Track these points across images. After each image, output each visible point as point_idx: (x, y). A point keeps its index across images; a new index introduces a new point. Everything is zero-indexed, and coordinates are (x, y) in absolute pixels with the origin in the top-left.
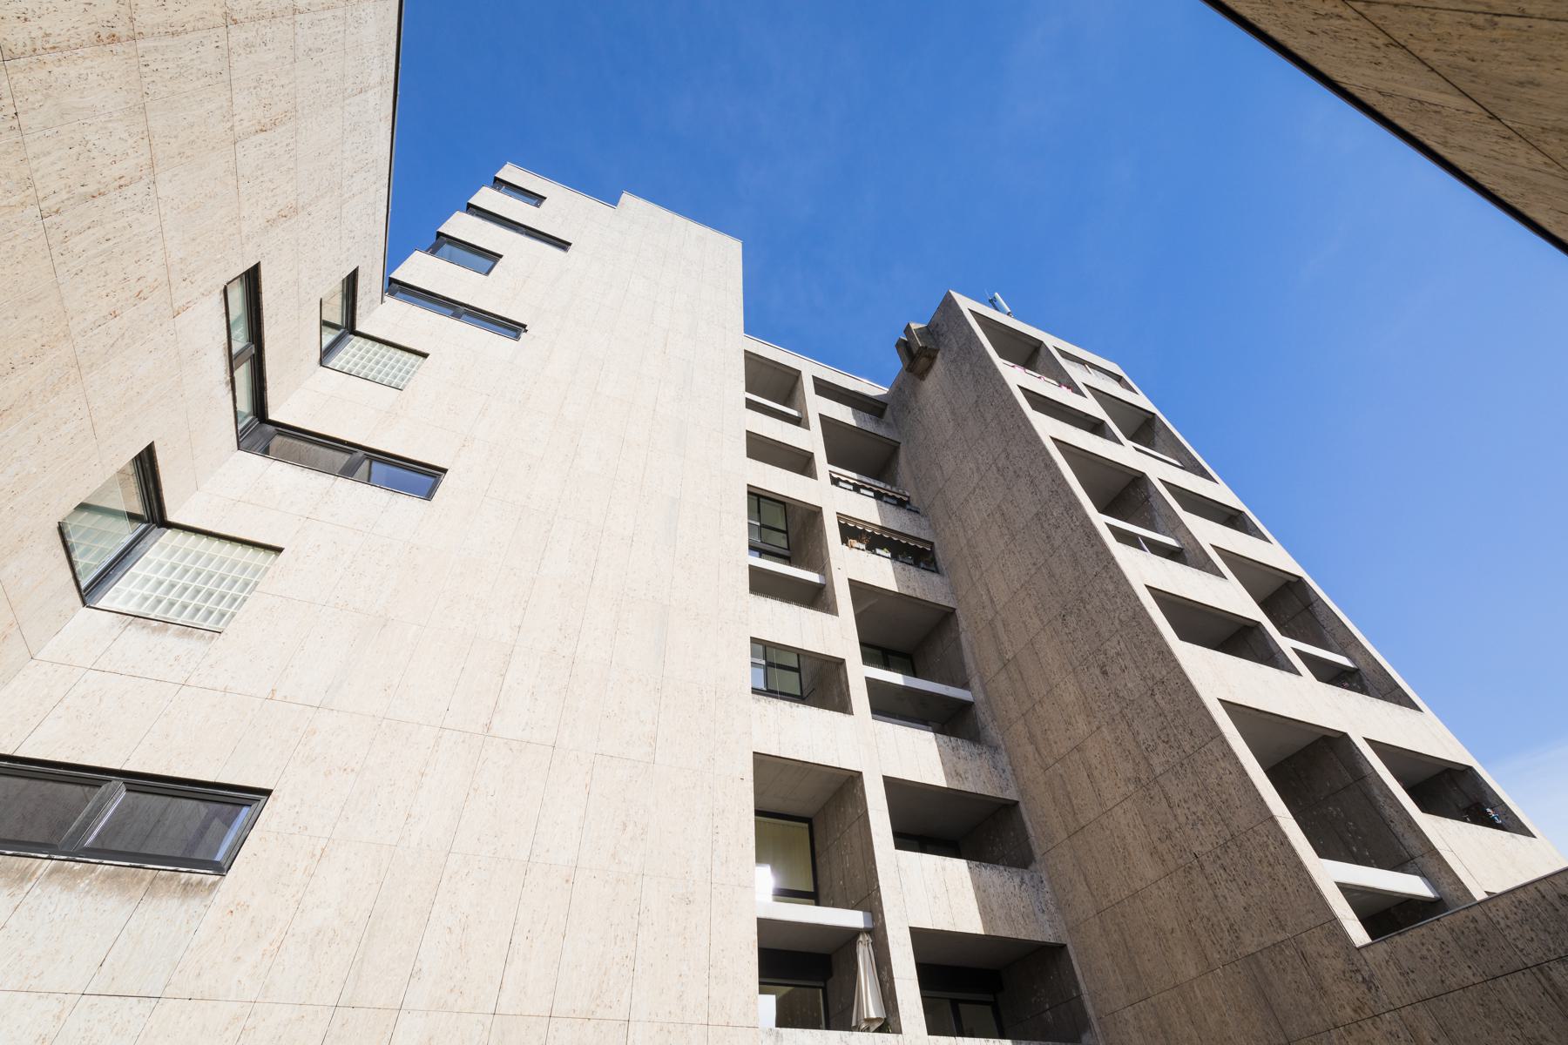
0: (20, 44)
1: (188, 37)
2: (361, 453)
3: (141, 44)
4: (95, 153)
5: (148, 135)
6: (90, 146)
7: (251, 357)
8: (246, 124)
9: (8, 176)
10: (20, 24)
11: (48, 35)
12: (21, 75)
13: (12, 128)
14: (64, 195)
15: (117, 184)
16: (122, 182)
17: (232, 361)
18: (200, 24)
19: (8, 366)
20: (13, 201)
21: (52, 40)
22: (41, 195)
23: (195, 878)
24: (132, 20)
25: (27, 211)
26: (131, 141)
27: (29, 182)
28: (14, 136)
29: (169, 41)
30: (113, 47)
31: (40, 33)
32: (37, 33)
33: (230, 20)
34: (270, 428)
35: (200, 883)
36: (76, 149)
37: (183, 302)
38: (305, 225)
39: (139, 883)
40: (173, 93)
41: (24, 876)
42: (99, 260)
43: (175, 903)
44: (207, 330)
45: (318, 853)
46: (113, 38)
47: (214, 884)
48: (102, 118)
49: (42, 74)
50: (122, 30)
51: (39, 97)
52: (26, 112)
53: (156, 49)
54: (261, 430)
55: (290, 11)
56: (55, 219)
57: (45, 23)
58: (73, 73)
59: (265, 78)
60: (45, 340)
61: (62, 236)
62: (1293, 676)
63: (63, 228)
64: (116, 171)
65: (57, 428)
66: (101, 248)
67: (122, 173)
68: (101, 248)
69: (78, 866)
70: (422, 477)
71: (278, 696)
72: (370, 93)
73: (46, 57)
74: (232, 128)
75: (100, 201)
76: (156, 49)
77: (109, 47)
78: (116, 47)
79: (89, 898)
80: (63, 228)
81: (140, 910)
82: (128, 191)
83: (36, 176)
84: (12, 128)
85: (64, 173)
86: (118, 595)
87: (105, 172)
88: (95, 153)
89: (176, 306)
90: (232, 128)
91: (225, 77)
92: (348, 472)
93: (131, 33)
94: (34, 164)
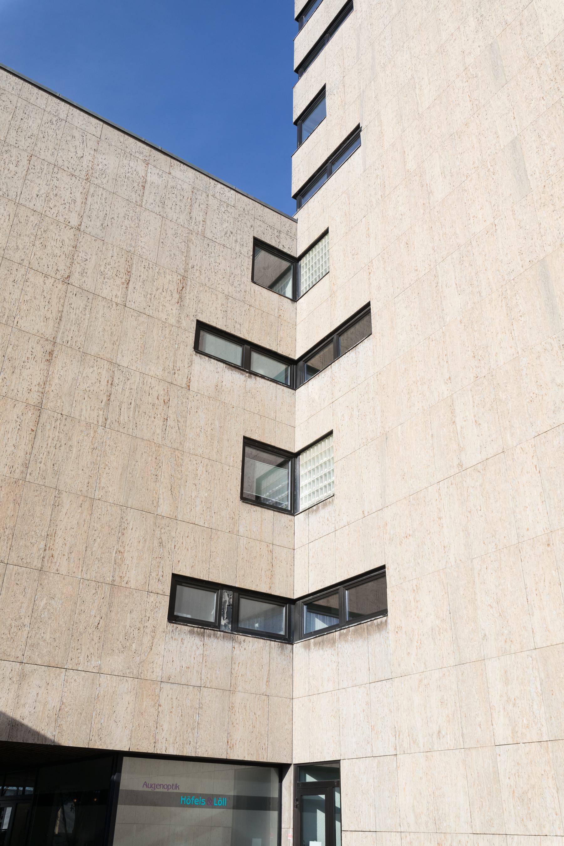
0: (38, 398)
1: (65, 312)
2: (335, 336)
3: (58, 341)
4: (92, 389)
5: (97, 357)
6: (88, 389)
7: (250, 351)
8: (119, 294)
9: (82, 431)
10: (31, 394)
11: (39, 384)
12: (49, 404)
13: (66, 419)
14: (101, 413)
15: (109, 385)
16: (110, 382)
17: (245, 367)
18: (62, 301)
19: (154, 477)
20: (92, 435)
21: (41, 383)
22: (96, 423)
23: (379, 620)
24: (47, 340)
25: (99, 432)
26: (95, 368)
27: (88, 425)
28: (69, 420)
29: (62, 323)
30: (54, 355)
31: (37, 386)
32: (37, 388)
33: (66, 281)
34: (301, 363)
35: (381, 622)
36: (86, 396)
37: (185, 380)
38: (197, 274)
39: (364, 631)
40: (86, 333)
41: (334, 642)
42: (137, 413)
43: (378, 635)
44: (210, 375)
45: (415, 588)
46: (51, 354)
47: (386, 621)
48: (80, 377)
49: (52, 395)
50: (49, 347)
51: (59, 401)
52: (62, 410)
53: (63, 333)
54: (298, 370)
55: (78, 232)
56: (108, 422)
57: (35, 383)
58: (57, 381)
59: (102, 269)
60: (154, 457)
61: (117, 424)
62: (329, 100)
63: (114, 421)
64: (104, 383)
65: (197, 475)
66: (132, 409)
67: (106, 380)
68: (132, 409)
69: (345, 631)
70: (360, 320)
71: (366, 514)
72: (149, 179)
73: (47, 389)
74: (117, 304)
75: (112, 398)
76: (63, 333)
77: (53, 358)
78: (55, 353)
79: (354, 643)
80: (114, 421)
81: (370, 643)
82: (116, 381)
83: (88, 420)
84: (66, 419)
85: (93, 408)
86: (303, 505)
87: (102, 388)
88: (92, 389)
89: (184, 385)
90: (117, 304)
91: (91, 296)
92: (337, 355)
93: (52, 343)
94: (83, 418)
